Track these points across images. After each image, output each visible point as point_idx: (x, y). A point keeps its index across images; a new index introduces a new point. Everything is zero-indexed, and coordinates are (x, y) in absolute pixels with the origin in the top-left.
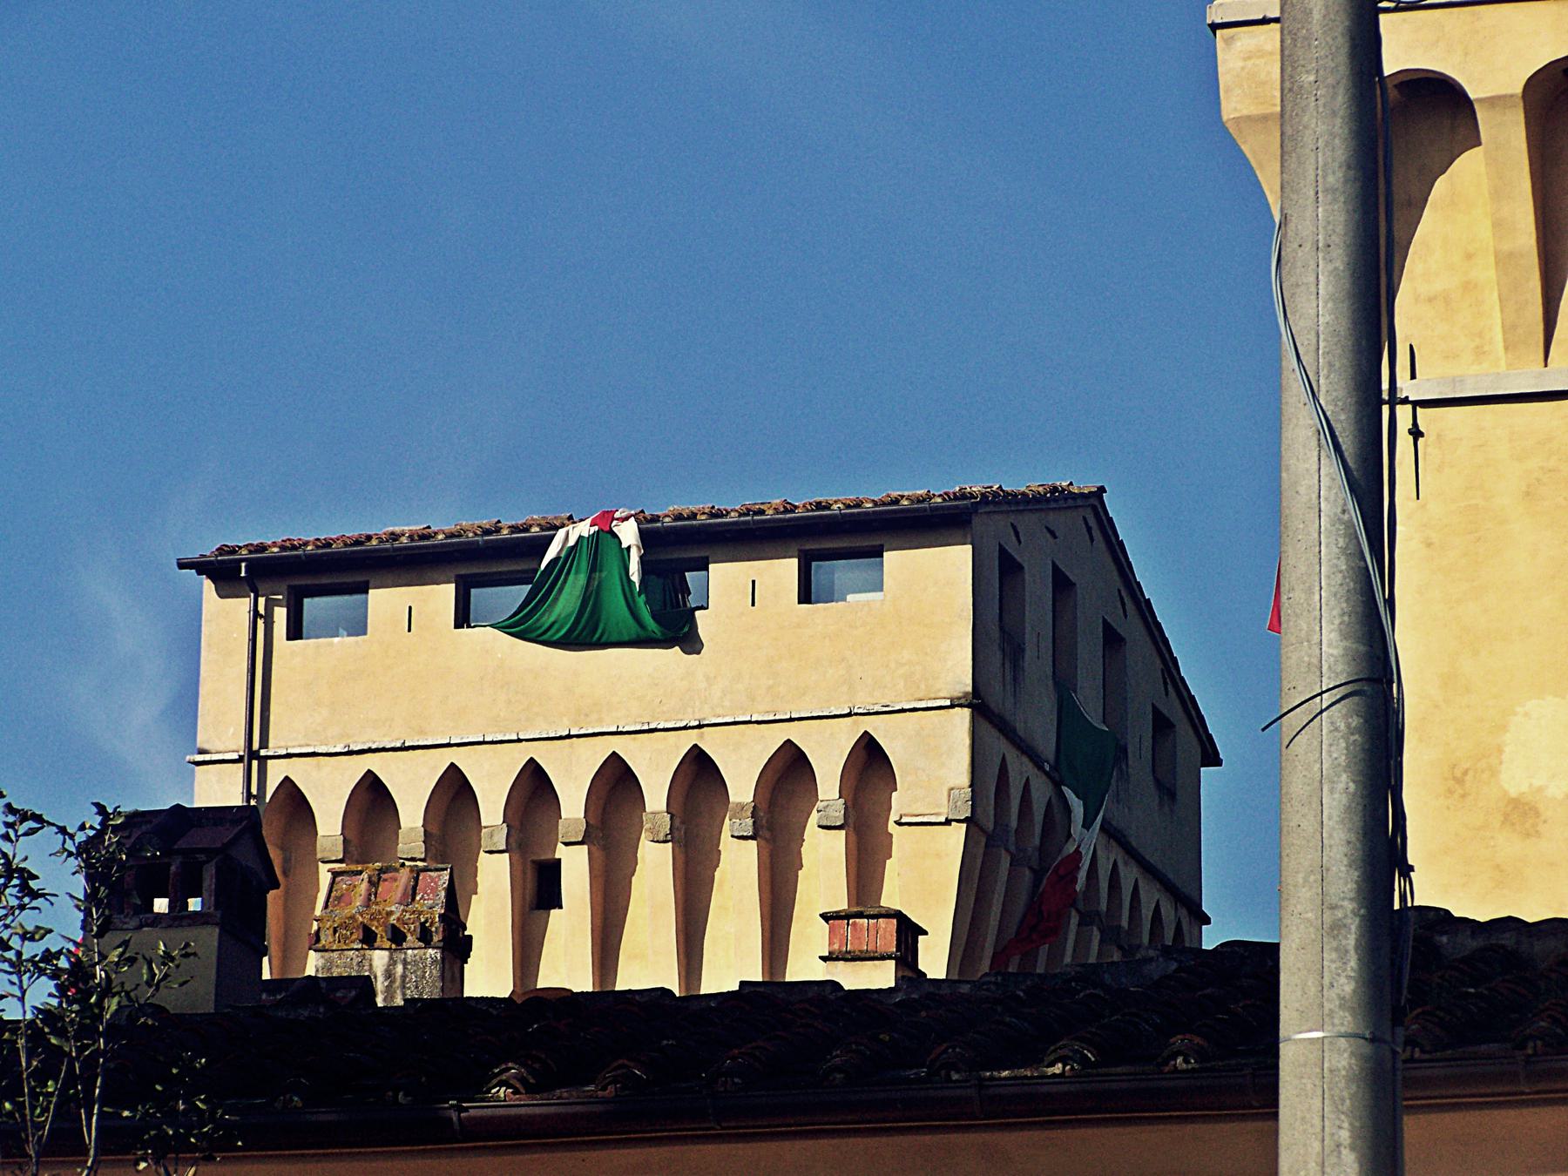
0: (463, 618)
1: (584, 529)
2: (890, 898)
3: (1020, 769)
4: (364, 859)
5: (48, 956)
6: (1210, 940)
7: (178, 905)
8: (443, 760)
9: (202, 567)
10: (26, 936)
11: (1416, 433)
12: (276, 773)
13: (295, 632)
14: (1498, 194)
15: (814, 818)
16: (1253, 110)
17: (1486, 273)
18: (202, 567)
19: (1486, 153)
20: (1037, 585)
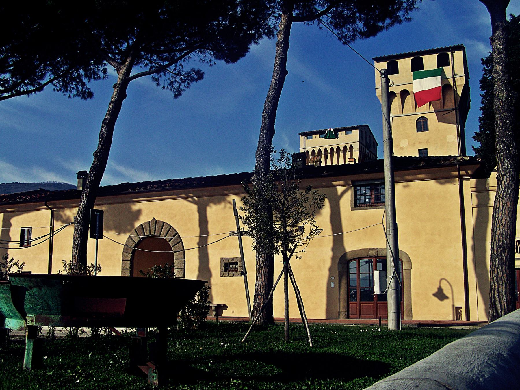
0: (320, 137)
1: (329, 130)
2: (353, 157)
3: (363, 147)
4: (313, 156)
5: (291, 164)
6: (378, 159)
7: (299, 160)
8: (319, 148)
9: (300, 134)
10: (289, 163)
11: (392, 119)
12: (306, 150)
13: (307, 139)
14: (398, 100)
15: (341, 152)
16: (379, 95)
17: (397, 107)
18: (300, 134)
19: (398, 98)
20: (364, 133)
